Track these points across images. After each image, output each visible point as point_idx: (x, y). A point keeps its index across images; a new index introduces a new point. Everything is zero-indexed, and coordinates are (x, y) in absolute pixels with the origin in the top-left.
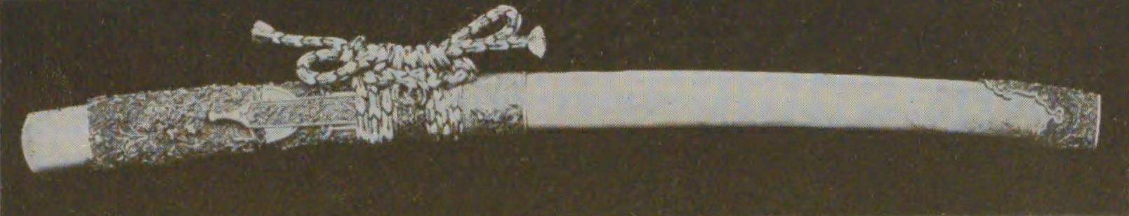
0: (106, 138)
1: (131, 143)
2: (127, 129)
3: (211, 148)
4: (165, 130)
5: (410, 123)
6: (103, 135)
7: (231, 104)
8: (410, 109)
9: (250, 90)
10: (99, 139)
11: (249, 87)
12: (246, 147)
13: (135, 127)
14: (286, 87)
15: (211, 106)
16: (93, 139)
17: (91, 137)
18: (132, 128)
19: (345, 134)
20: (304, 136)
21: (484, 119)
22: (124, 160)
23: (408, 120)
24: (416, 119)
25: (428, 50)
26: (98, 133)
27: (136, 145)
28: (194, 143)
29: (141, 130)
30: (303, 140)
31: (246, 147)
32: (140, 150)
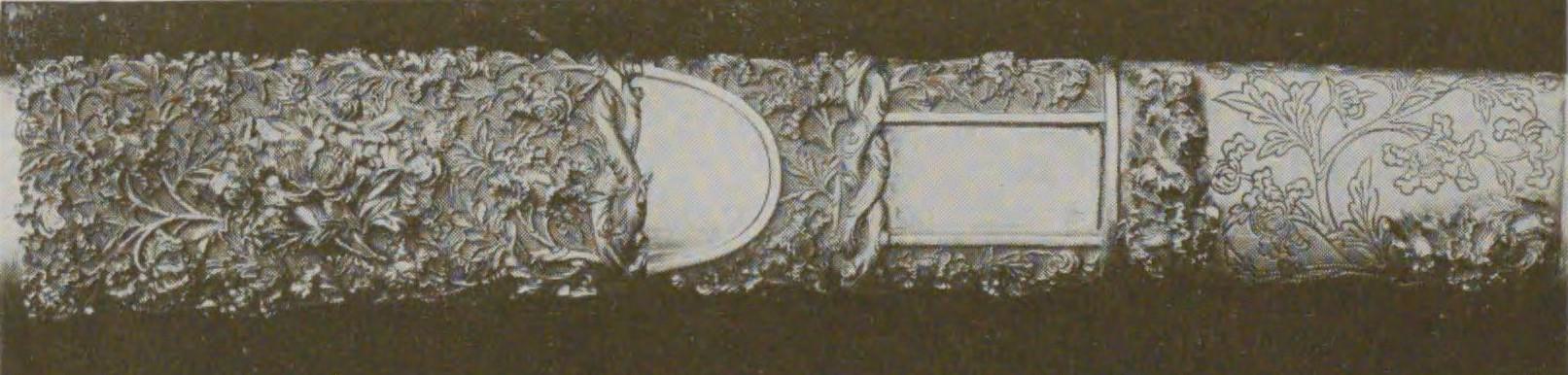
0: (79, 220)
1: (166, 241)
2: (157, 194)
3: (189, 263)
4: (290, 209)
5: (1175, 256)
6: (66, 207)
7: (533, 130)
8: (1180, 206)
9: (602, 82)
10: (53, 220)
11: (594, 65)
12: (575, 282)
13: (183, 185)
14: (719, 77)
15: (459, 130)
16: (34, 219)
17: (28, 209)
18: (172, 188)
19: (926, 261)
20: (782, 260)
21: (1433, 257)
22: (133, 299)
23: (1168, 246)
24: (1195, 242)
25: (1134, 250)
26: (50, 199)
27: (187, 248)
28: (390, 262)
29: (204, 198)
30: (776, 270)
31: (575, 282)
32: (198, 272)
